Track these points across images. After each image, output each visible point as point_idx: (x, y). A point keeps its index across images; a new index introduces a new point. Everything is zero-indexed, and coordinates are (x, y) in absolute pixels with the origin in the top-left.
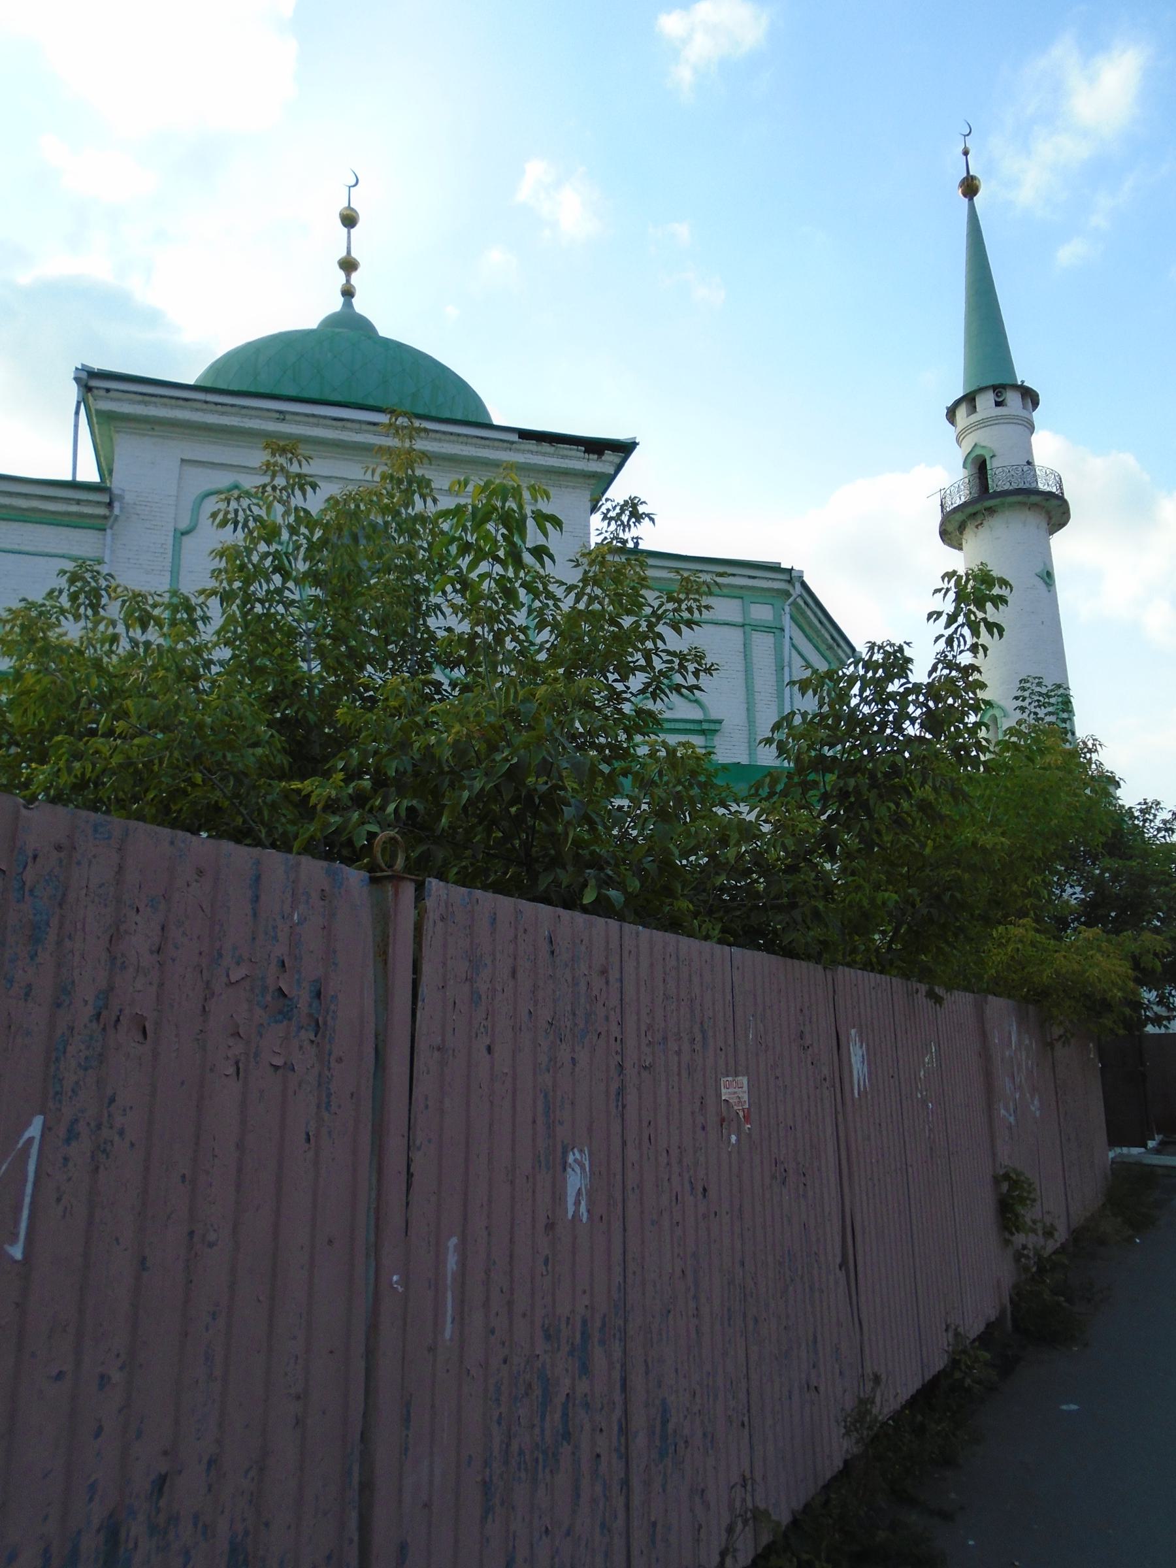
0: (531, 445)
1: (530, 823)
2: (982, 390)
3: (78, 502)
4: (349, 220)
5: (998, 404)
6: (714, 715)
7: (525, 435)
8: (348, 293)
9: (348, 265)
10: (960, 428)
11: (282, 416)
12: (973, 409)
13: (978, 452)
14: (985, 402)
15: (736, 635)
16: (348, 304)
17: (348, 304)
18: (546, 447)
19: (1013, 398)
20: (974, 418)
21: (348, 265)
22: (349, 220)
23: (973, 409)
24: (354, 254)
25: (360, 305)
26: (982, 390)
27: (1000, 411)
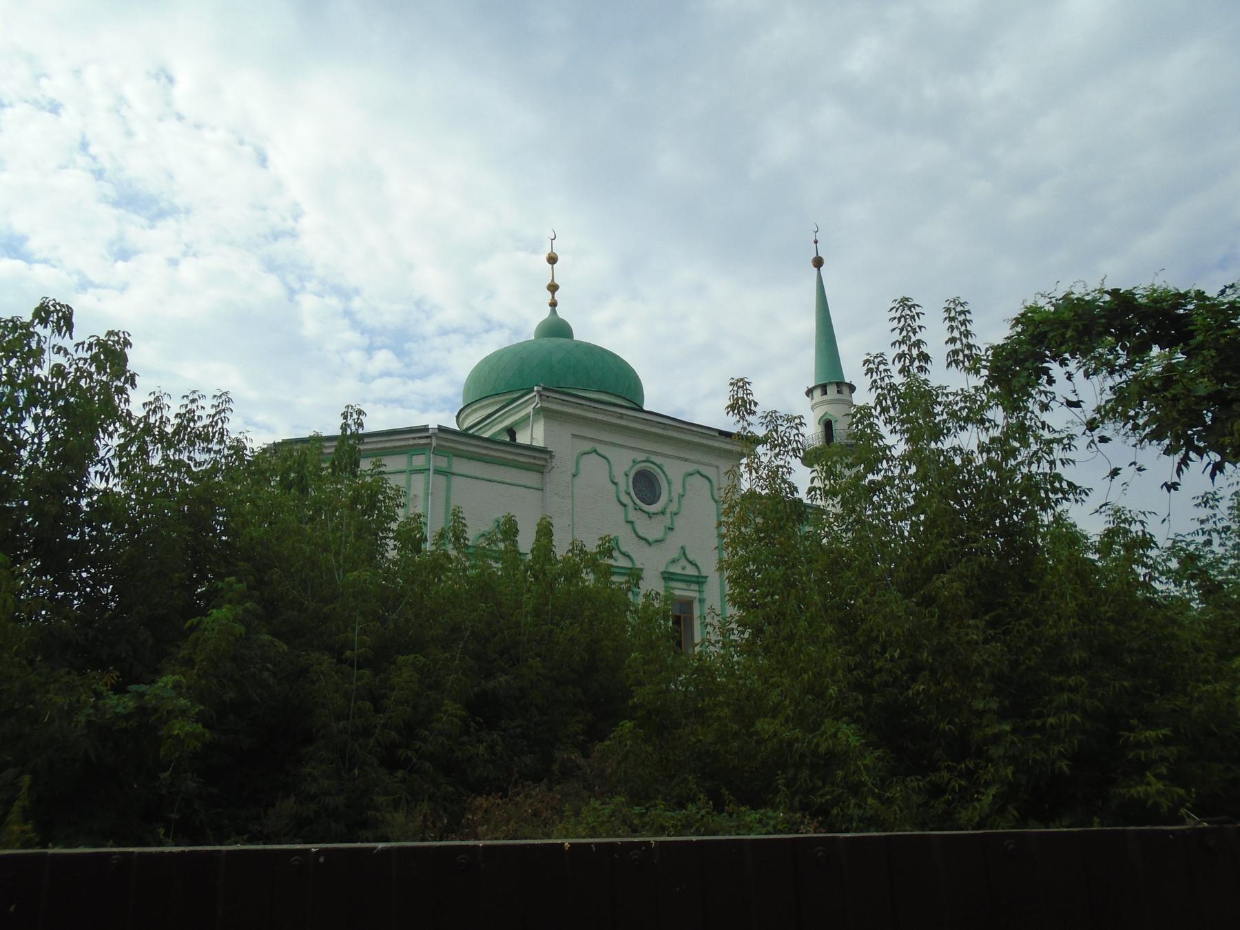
0: (722, 438)
1: (206, 421)
2: (831, 383)
3: (535, 458)
4: (552, 260)
5: (839, 392)
6: (638, 565)
7: (722, 433)
8: (553, 304)
9: (553, 288)
10: (815, 401)
11: (621, 416)
12: (825, 393)
13: (828, 417)
14: (832, 390)
16: (554, 312)
17: (554, 312)
19: (846, 390)
20: (825, 398)
21: (553, 288)
22: (552, 260)
23: (825, 393)
24: (556, 281)
25: (562, 312)
26: (831, 383)
27: (839, 396)
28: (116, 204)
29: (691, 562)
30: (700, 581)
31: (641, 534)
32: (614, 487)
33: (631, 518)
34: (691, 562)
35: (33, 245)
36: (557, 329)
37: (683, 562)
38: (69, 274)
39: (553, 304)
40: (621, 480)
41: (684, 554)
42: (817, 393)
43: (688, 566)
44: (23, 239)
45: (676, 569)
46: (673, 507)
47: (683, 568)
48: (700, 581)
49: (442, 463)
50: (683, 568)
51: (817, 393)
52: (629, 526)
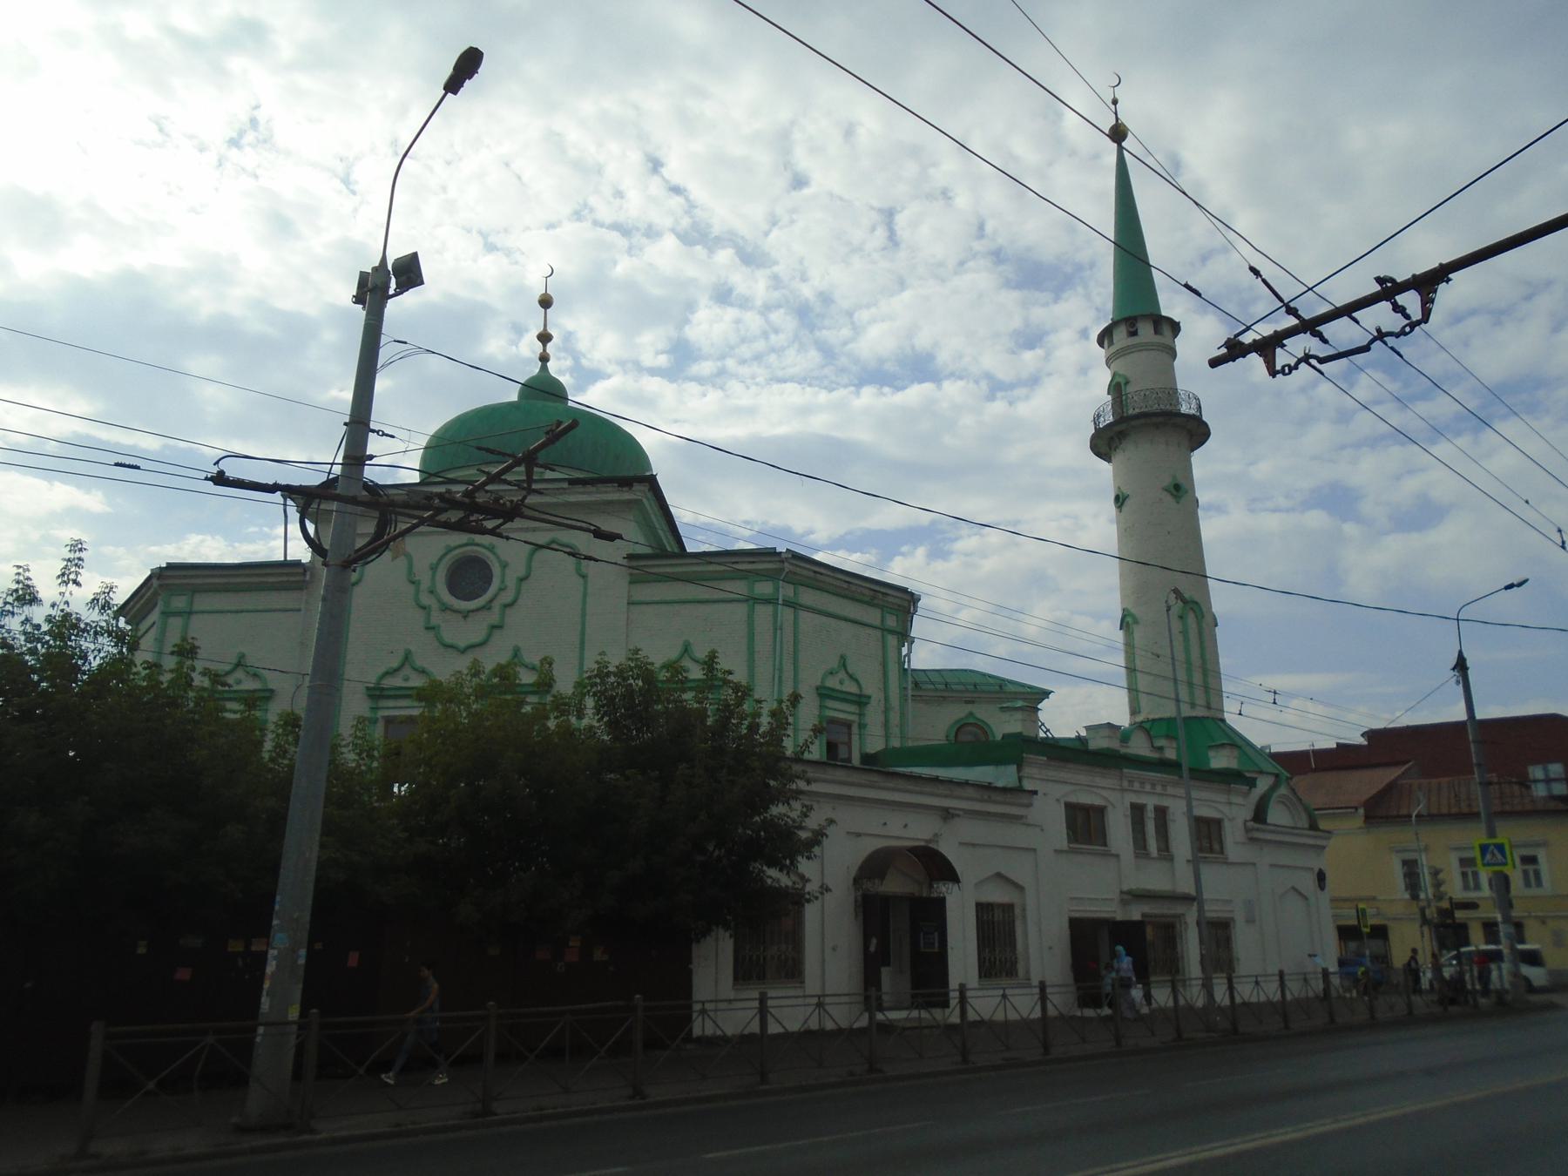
0: (579, 488)
8: (544, 359)
15: (741, 610)
17: (544, 368)
18: (590, 488)
23: (1134, 334)
28: (1019, 286)
29: (851, 677)
30: (861, 701)
31: (462, 644)
32: (412, 588)
33: (434, 622)
34: (851, 677)
35: (943, 357)
36: (543, 389)
37: (842, 675)
38: (977, 382)
39: (544, 359)
40: (425, 579)
41: (844, 666)
42: (1120, 336)
43: (847, 682)
44: (930, 357)
45: (832, 683)
46: (507, 597)
47: (841, 683)
48: (861, 701)
49: (787, 591)
50: (841, 683)
51: (1120, 336)
52: (431, 634)
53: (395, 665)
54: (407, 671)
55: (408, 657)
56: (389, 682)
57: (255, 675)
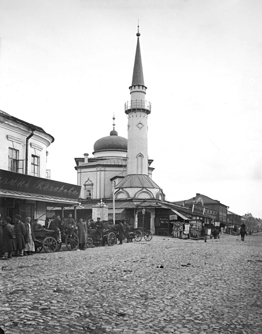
8: (114, 128)
16: (114, 129)
17: (114, 129)
26: (137, 85)
36: (113, 133)
48: (92, 185)
53: (87, 180)
54: (89, 181)
55: (89, 179)
56: (87, 183)
57: (91, 181)
